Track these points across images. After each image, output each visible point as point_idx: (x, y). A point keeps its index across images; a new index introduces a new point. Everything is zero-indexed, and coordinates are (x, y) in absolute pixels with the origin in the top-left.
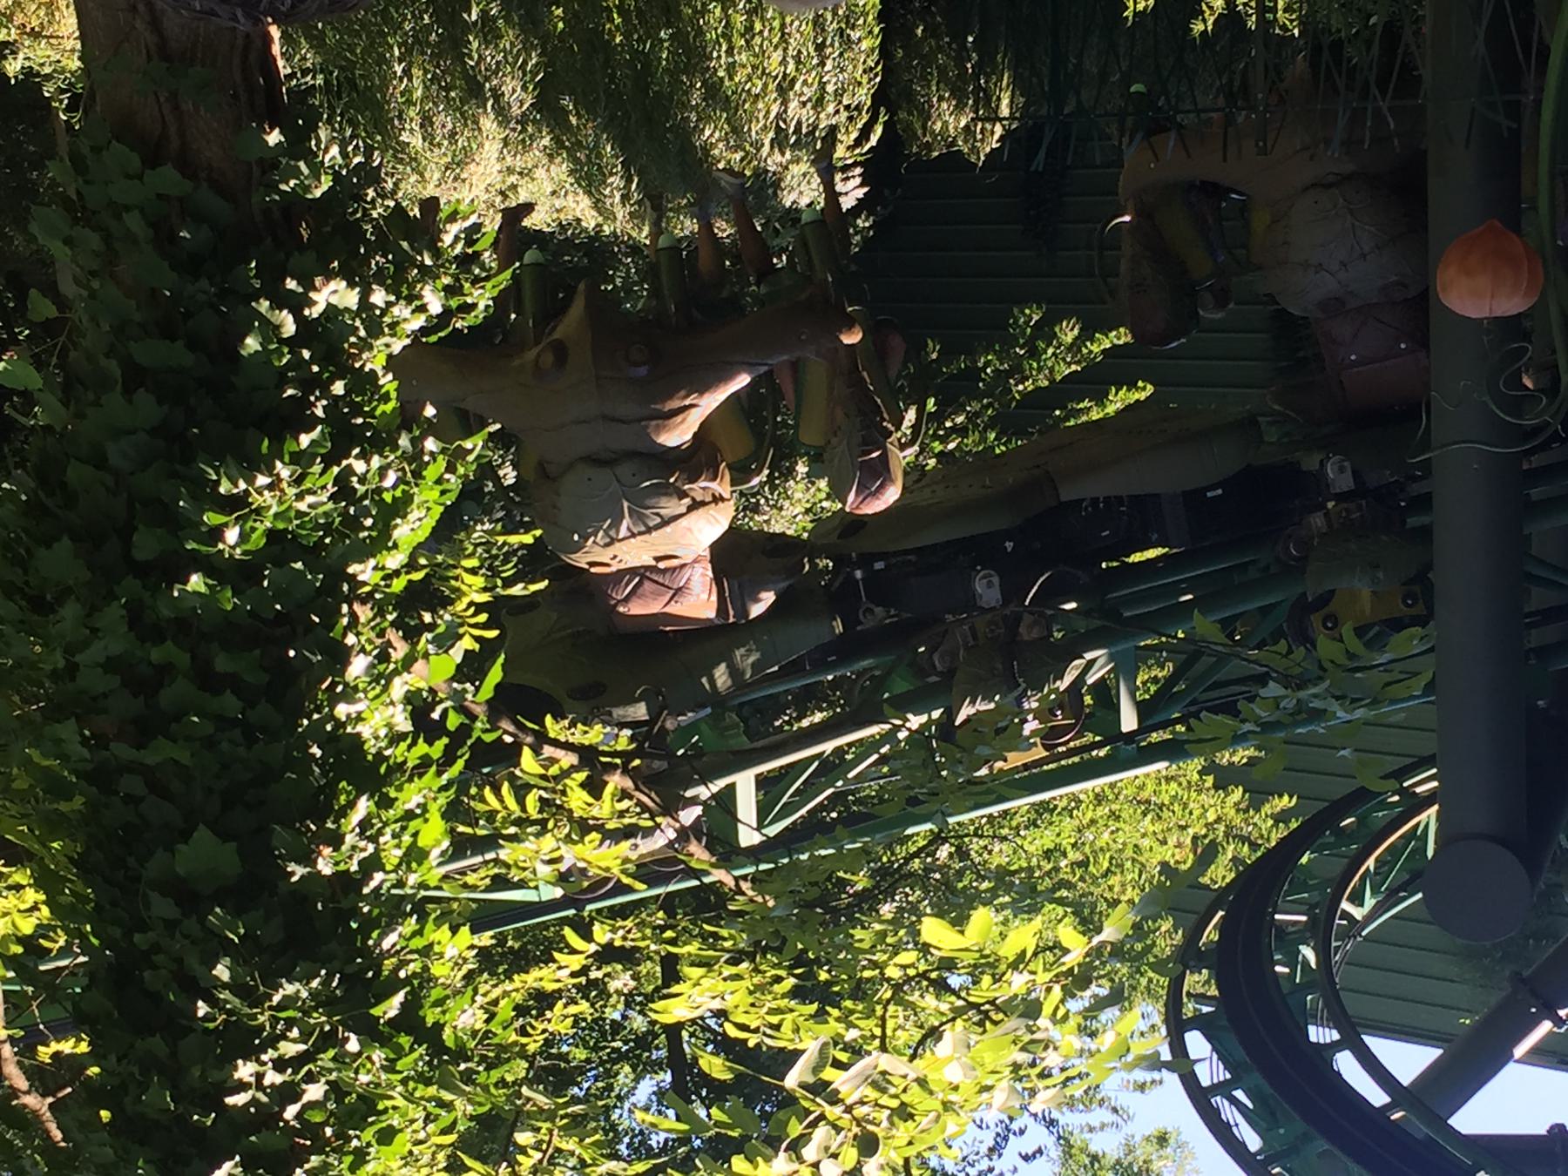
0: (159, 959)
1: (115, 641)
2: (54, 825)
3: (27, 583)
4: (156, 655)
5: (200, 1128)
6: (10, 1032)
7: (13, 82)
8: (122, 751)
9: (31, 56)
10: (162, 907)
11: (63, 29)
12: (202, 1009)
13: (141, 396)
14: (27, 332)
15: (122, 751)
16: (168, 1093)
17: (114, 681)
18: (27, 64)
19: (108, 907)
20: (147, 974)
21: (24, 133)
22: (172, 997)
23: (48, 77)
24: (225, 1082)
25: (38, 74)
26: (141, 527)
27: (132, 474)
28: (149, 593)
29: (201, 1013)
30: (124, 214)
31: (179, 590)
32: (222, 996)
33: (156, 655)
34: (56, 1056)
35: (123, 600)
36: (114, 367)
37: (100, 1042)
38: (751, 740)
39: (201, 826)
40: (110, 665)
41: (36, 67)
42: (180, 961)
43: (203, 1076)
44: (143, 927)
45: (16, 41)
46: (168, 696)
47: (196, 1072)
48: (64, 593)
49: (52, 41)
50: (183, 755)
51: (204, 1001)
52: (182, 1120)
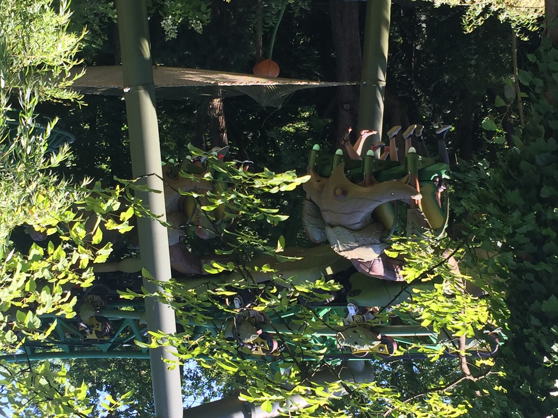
0: (531, 339)
1: (530, 224)
2: (499, 287)
3: (501, 201)
4: (544, 232)
6: (467, 354)
7: (502, 22)
8: (527, 264)
9: (509, 14)
10: (535, 321)
11: (522, 4)
12: (546, 359)
13: (552, 140)
14: (491, 110)
15: (527, 264)
16: (530, 387)
17: (528, 240)
18: (507, 16)
19: (515, 318)
20: (526, 344)
21: (499, 40)
22: (535, 354)
23: (514, 21)
24: (550, 386)
25: (510, 20)
26: (545, 186)
27: (543, 167)
28: (544, 210)
29: (545, 361)
30: (553, 74)
31: (556, 210)
32: (554, 357)
33: (544, 232)
34: (483, 365)
35: (535, 212)
36: (542, 128)
37: (506, 364)
38: (361, 167)
39: (553, 295)
40: (528, 234)
41: (510, 18)
42: (539, 341)
43: (543, 384)
44: (527, 327)
45: (504, 8)
46: (547, 247)
48: (515, 207)
49: (517, 8)
50: (550, 270)
51: (547, 357)
52: (533, 397)
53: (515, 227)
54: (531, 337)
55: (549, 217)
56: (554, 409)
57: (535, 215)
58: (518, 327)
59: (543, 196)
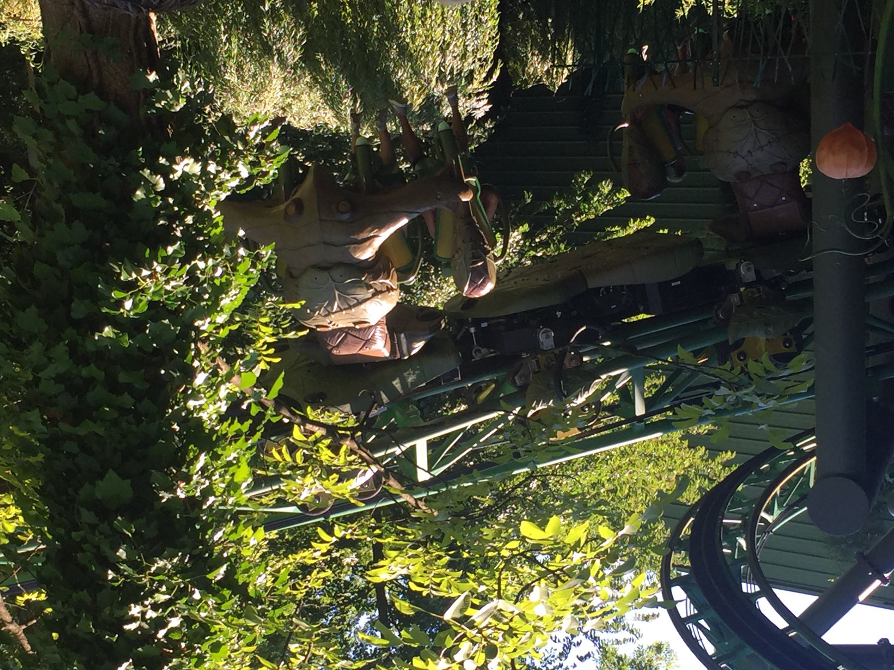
0: (85, 546)
1: (61, 363)
2: (26, 470)
3: (11, 331)
4: (84, 372)
5: (110, 643)
8: (65, 427)
9: (14, 31)
10: (88, 517)
12: (111, 575)
14: (11, 188)
15: (65, 427)
16: (91, 623)
17: (61, 387)
18: (12, 35)
22: (94, 569)
23: (24, 43)
25: (18, 41)
29: (110, 577)
32: (122, 568)
33: (84, 372)
34: (27, 602)
36: (60, 208)
37: (52, 594)
39: (111, 470)
40: (58, 379)
41: (17, 38)
42: (98, 548)
43: (111, 614)
44: (76, 528)
47: (107, 611)
48: (32, 338)
50: (101, 431)
51: (112, 570)
52: (99, 639)
53: (36, 370)
54: (84, 544)
55: (90, 348)
56: (134, 651)
57: (66, 345)
58: (62, 531)
59: (75, 315)
